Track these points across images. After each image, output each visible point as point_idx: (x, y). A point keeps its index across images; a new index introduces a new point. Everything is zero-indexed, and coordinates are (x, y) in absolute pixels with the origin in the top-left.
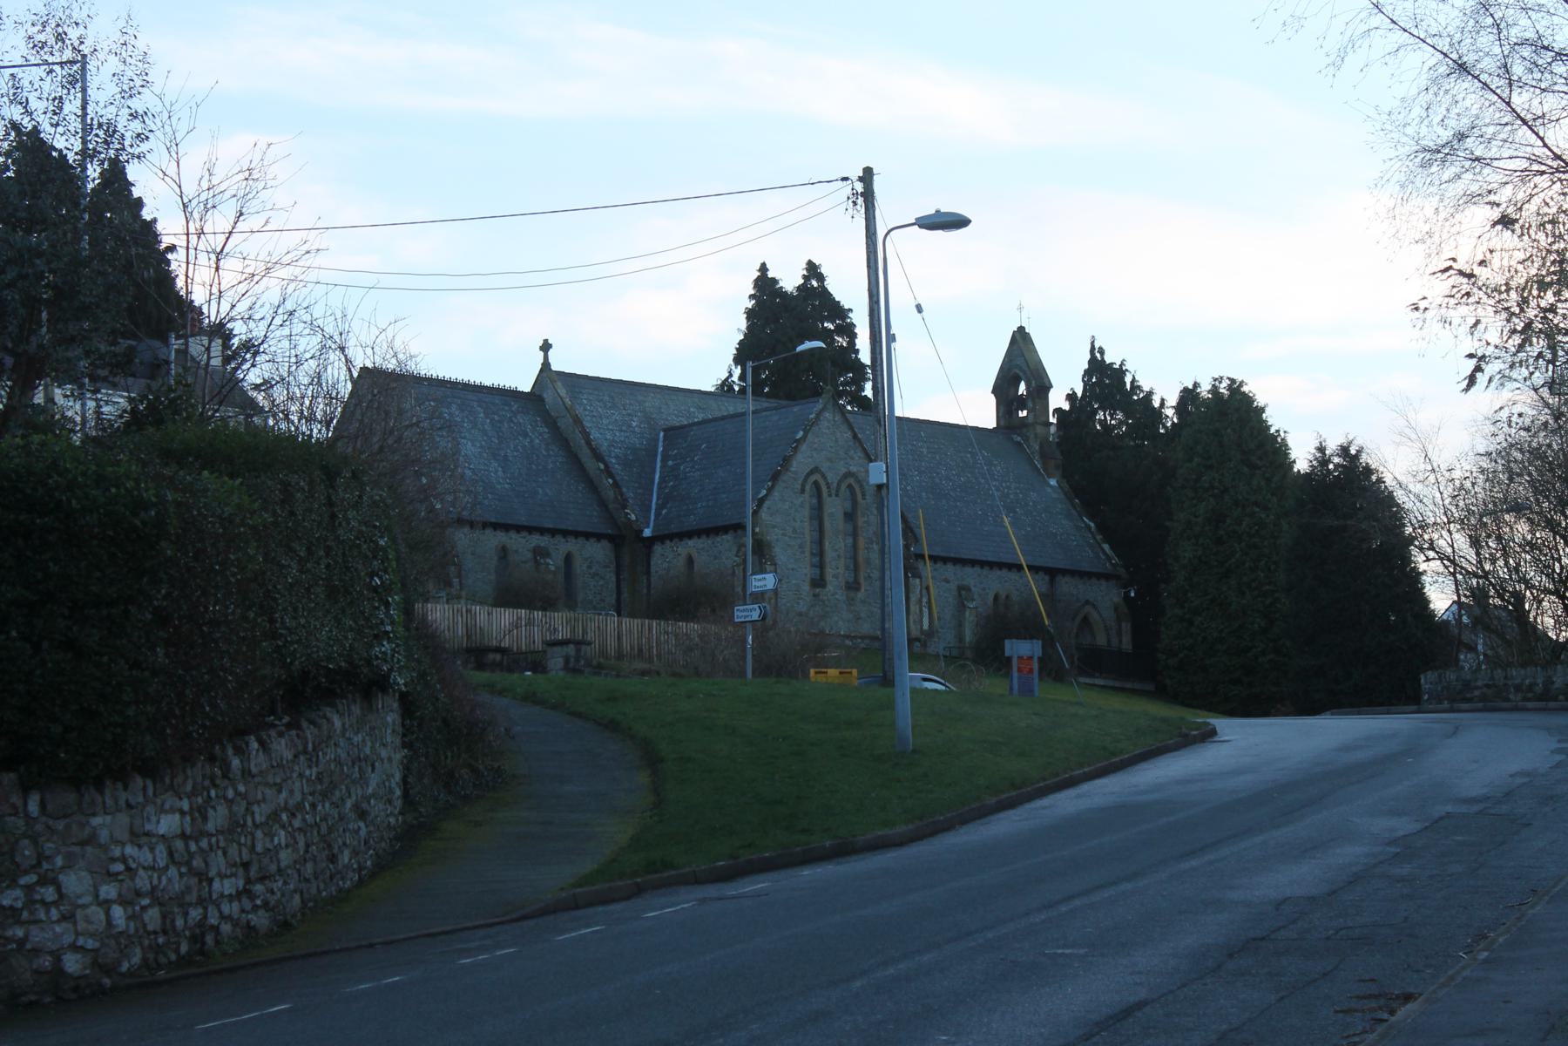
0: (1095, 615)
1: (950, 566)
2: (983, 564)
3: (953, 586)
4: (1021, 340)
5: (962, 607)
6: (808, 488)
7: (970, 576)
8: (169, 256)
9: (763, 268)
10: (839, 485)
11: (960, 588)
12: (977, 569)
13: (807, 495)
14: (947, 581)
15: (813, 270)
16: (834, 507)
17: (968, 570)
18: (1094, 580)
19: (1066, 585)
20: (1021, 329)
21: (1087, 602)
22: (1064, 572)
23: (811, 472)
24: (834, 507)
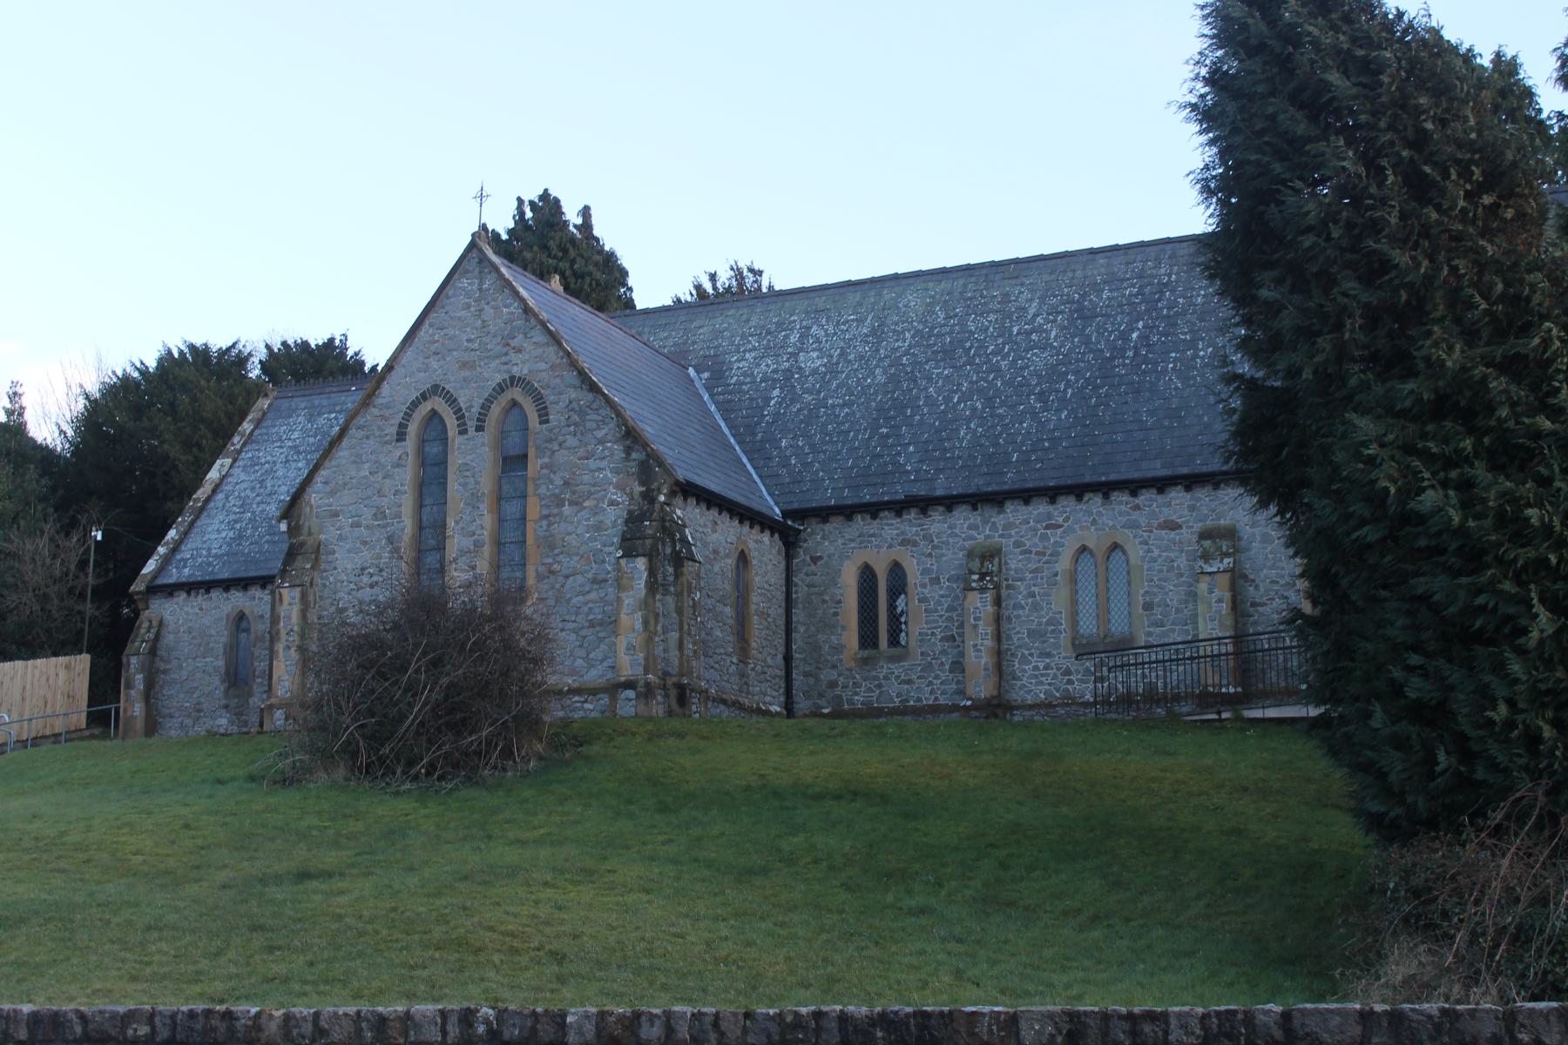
1: (1177, 495)
3: (1188, 535)
6: (413, 428)
10: (486, 407)
13: (410, 444)
14: (1173, 526)
16: (471, 457)
23: (436, 390)
24: (471, 457)
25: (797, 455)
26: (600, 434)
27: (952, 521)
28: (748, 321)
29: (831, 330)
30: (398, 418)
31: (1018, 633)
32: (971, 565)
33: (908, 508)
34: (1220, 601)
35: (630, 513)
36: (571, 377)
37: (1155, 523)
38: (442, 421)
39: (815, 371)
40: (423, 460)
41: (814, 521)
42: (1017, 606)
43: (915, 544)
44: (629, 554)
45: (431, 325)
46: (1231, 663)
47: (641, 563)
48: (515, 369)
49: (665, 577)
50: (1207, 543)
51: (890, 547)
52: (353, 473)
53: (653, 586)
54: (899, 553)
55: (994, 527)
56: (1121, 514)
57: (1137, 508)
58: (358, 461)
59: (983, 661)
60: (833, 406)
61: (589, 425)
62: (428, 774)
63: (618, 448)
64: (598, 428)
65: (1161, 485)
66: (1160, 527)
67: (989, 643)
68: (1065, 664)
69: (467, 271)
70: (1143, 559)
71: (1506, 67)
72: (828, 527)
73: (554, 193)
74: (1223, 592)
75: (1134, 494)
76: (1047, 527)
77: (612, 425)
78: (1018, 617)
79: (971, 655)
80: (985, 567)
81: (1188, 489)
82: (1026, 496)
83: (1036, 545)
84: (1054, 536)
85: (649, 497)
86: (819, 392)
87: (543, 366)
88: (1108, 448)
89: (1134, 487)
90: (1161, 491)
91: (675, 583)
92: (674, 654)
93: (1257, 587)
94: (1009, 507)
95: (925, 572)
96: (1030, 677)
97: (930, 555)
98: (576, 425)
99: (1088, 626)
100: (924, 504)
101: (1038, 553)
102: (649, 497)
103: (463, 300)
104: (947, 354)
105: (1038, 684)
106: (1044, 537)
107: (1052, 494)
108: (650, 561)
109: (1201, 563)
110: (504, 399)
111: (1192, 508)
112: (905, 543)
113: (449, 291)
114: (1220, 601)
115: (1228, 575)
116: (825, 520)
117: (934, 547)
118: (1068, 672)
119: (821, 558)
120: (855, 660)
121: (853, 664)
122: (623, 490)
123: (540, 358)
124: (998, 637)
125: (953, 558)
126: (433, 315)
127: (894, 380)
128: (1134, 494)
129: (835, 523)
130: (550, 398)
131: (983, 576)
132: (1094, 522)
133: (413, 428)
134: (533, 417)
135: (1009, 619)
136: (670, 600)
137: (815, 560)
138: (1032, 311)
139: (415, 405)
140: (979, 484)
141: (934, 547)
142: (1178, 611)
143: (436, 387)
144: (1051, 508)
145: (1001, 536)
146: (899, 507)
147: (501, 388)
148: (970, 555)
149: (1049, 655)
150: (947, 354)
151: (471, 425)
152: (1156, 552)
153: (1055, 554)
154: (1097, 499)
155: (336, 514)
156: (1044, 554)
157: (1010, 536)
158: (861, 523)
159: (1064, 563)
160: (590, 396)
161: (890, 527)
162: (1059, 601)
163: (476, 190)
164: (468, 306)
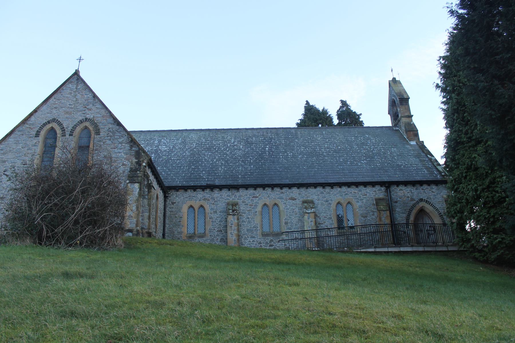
0: (428, 208)
1: (295, 190)
2: (324, 185)
3: (299, 202)
4: (394, 83)
6: (43, 133)
9: (307, 103)
10: (74, 128)
13: (41, 138)
14: (294, 199)
15: (344, 103)
17: (312, 190)
18: (425, 186)
21: (421, 200)
22: (398, 183)
23: (54, 120)
25: (164, 172)
26: (120, 140)
27: (222, 193)
28: (140, 137)
29: (168, 141)
30: (37, 129)
31: (244, 230)
32: (229, 207)
33: (206, 188)
34: (311, 221)
35: (131, 168)
36: (111, 120)
37: (288, 198)
38: (55, 132)
39: (165, 151)
40: (45, 145)
41: (173, 191)
42: (243, 221)
43: (209, 200)
44: (132, 182)
45: (55, 98)
46: (316, 241)
47: (137, 186)
48: (88, 116)
49: (144, 192)
50: (306, 204)
51: (200, 200)
52: (14, 147)
53: (141, 195)
54: (202, 203)
55: (235, 196)
56: (277, 194)
57: (282, 193)
58: (17, 143)
59: (234, 238)
60: (174, 160)
61: (116, 137)
62: (81, 244)
63: (127, 146)
64: (120, 138)
65: (290, 186)
66: (290, 199)
67: (236, 232)
68: (259, 240)
69: (72, 82)
70: (284, 208)
71: (325, 112)
72: (178, 193)
74: (312, 219)
75: (281, 188)
76: (253, 197)
77: (126, 138)
78: (244, 225)
79: (229, 235)
80: (233, 208)
81: (298, 188)
82: (246, 187)
83: (249, 203)
85: (139, 163)
86: (168, 156)
87: (99, 116)
88: (270, 176)
89: (281, 186)
90: (290, 188)
91: (148, 195)
92: (146, 221)
93: (320, 219)
94: (241, 190)
95: (212, 209)
96: (248, 244)
97: (214, 204)
98: (111, 136)
99: (266, 229)
100: (212, 187)
101: (250, 205)
102: (139, 163)
103: (69, 91)
104: (209, 149)
106: (252, 200)
107: (255, 187)
108: (140, 185)
109: (305, 210)
110: (82, 126)
111: (299, 194)
112: (205, 199)
113: (64, 87)
114: (311, 221)
115: (314, 214)
116: (177, 191)
117: (215, 201)
118: (260, 243)
119: (175, 203)
120: (187, 237)
121: (186, 238)
122: (129, 160)
123: (98, 113)
124: (238, 230)
125: (221, 205)
126: (55, 95)
127: (193, 155)
128: (281, 188)
129: (181, 192)
130: (101, 126)
131: (233, 211)
132: (269, 196)
133: (43, 133)
134: (93, 133)
135: (241, 225)
136: (146, 201)
137: (173, 203)
138: (233, 141)
139: (45, 125)
140: (230, 182)
141: (215, 201)
142: (296, 225)
143: (55, 119)
144: (254, 191)
145: (238, 199)
146: (203, 188)
147: (81, 122)
148: (228, 204)
149: (254, 237)
150: (209, 149)
151: (67, 133)
152: (288, 207)
153: (256, 206)
154: (270, 190)
155: (5, 162)
156: (252, 205)
157: (241, 199)
158: (190, 192)
159: (259, 208)
160: (118, 127)
161: (200, 194)
162: (257, 220)
163: (78, 57)
164: (71, 93)
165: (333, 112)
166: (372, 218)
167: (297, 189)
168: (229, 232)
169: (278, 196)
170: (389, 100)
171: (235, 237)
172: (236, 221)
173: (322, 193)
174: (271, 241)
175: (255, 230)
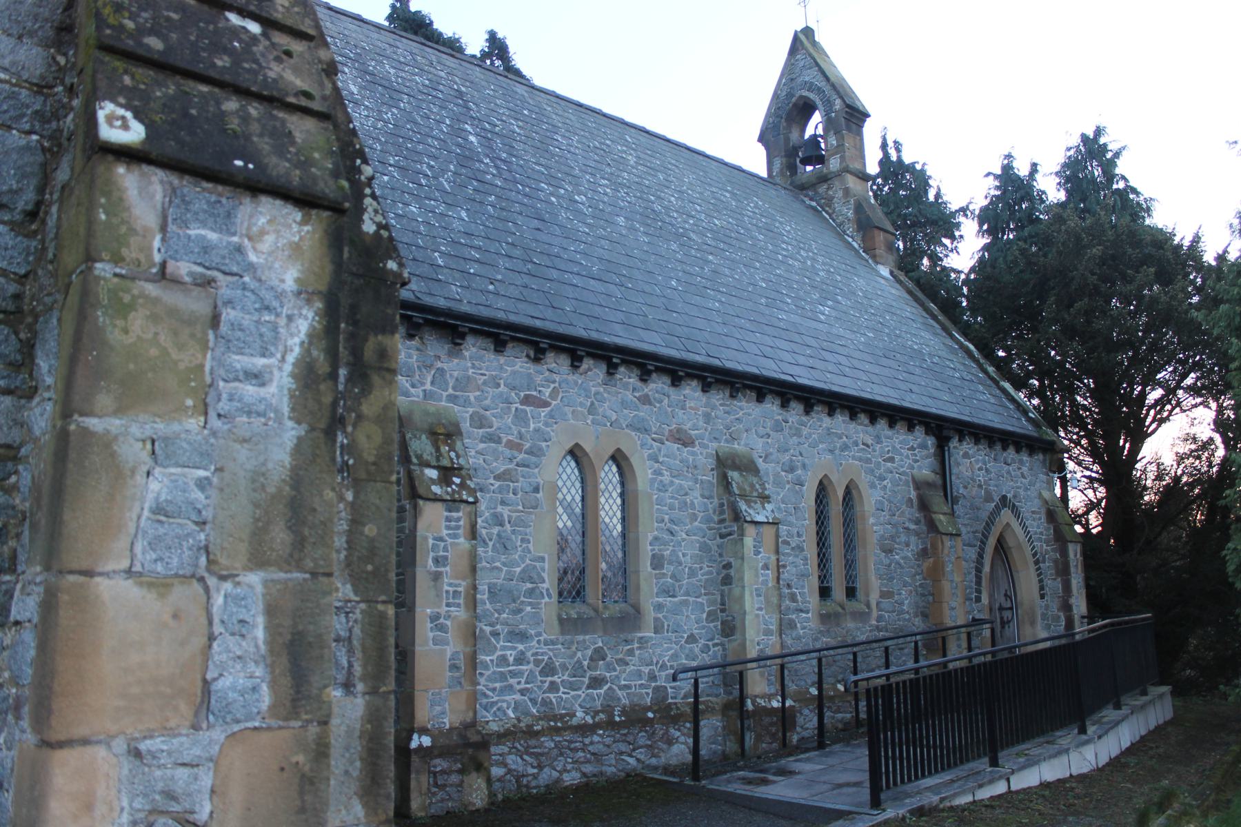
1: (691, 391)
3: (702, 456)
4: (803, 45)
5: (732, 519)
7: (754, 426)
8: (1102, 141)
11: (725, 464)
12: (771, 407)
14: (684, 440)
17: (747, 408)
19: (969, 461)
20: (808, 32)
34: (766, 567)
56: (624, 404)
57: (645, 400)
59: (449, 651)
67: (461, 613)
68: (546, 653)
70: (652, 481)
73: (1111, 140)
76: (527, 400)
79: (424, 632)
84: (537, 419)
94: (472, 347)
101: (510, 445)
105: (503, 691)
106: (520, 418)
111: (707, 418)
118: (549, 670)
132: (592, 410)
144: (531, 368)
145: (452, 399)
149: (523, 637)
152: (666, 478)
157: (467, 403)
165: (475, 45)
166: (904, 558)
167: (699, 394)
168: (424, 610)
169: (630, 414)
170: (776, 95)
171: (453, 647)
172: (463, 543)
173: (778, 428)
174: (599, 655)
175: (530, 593)
